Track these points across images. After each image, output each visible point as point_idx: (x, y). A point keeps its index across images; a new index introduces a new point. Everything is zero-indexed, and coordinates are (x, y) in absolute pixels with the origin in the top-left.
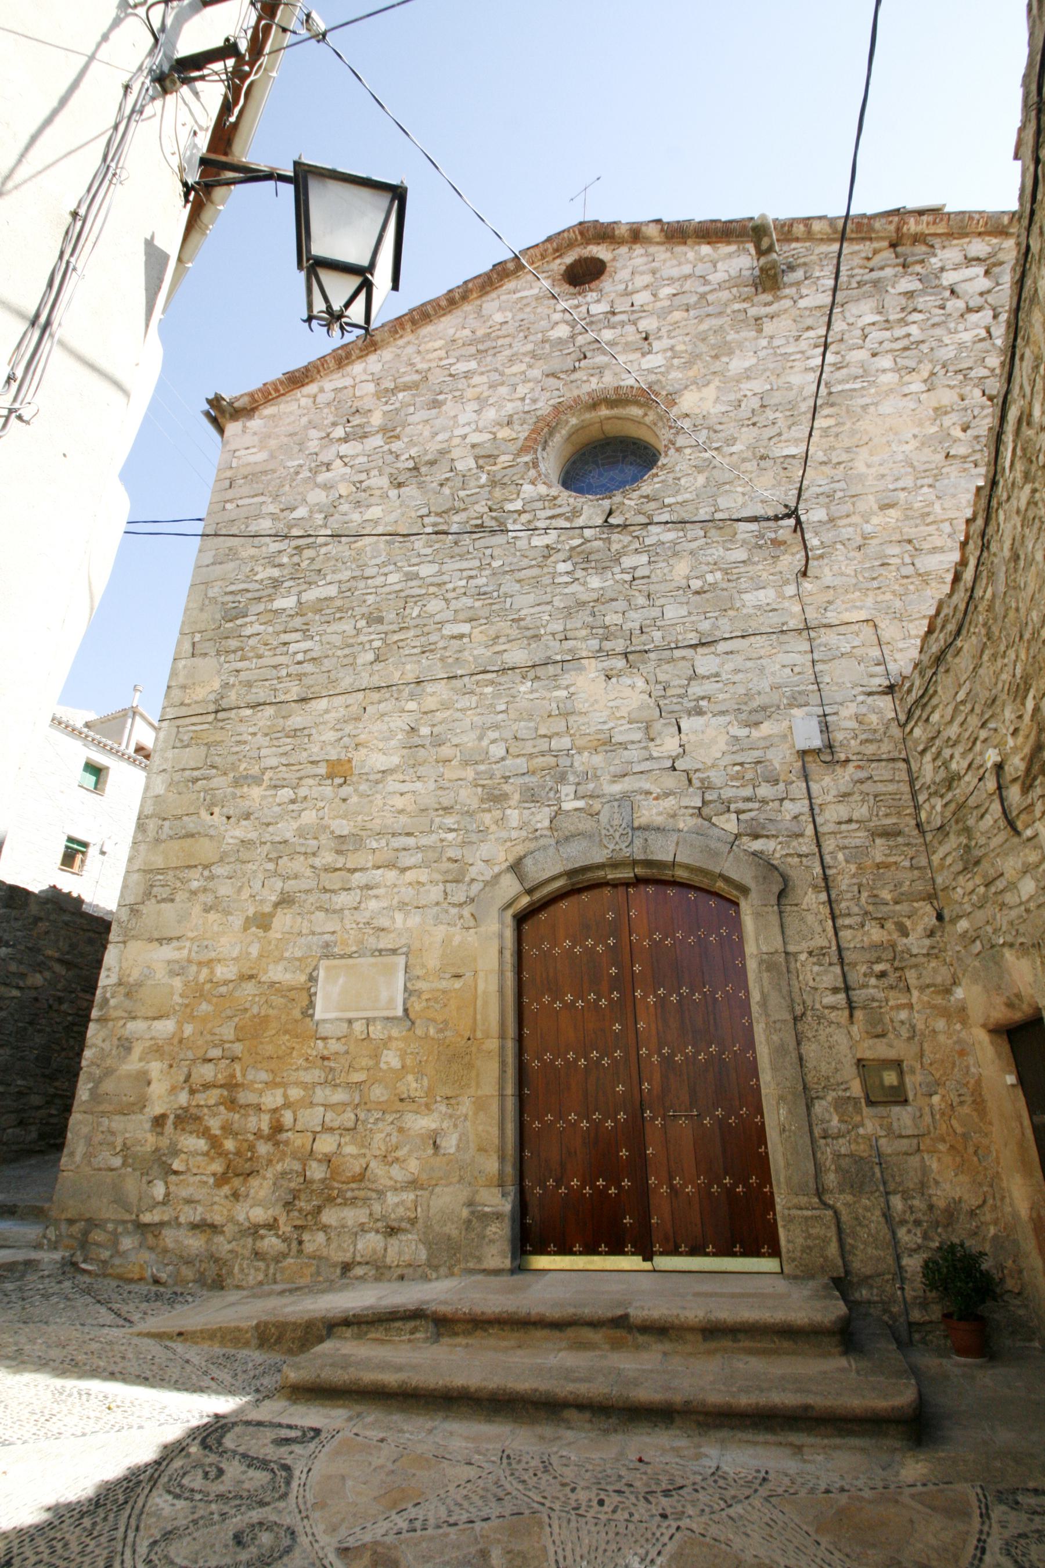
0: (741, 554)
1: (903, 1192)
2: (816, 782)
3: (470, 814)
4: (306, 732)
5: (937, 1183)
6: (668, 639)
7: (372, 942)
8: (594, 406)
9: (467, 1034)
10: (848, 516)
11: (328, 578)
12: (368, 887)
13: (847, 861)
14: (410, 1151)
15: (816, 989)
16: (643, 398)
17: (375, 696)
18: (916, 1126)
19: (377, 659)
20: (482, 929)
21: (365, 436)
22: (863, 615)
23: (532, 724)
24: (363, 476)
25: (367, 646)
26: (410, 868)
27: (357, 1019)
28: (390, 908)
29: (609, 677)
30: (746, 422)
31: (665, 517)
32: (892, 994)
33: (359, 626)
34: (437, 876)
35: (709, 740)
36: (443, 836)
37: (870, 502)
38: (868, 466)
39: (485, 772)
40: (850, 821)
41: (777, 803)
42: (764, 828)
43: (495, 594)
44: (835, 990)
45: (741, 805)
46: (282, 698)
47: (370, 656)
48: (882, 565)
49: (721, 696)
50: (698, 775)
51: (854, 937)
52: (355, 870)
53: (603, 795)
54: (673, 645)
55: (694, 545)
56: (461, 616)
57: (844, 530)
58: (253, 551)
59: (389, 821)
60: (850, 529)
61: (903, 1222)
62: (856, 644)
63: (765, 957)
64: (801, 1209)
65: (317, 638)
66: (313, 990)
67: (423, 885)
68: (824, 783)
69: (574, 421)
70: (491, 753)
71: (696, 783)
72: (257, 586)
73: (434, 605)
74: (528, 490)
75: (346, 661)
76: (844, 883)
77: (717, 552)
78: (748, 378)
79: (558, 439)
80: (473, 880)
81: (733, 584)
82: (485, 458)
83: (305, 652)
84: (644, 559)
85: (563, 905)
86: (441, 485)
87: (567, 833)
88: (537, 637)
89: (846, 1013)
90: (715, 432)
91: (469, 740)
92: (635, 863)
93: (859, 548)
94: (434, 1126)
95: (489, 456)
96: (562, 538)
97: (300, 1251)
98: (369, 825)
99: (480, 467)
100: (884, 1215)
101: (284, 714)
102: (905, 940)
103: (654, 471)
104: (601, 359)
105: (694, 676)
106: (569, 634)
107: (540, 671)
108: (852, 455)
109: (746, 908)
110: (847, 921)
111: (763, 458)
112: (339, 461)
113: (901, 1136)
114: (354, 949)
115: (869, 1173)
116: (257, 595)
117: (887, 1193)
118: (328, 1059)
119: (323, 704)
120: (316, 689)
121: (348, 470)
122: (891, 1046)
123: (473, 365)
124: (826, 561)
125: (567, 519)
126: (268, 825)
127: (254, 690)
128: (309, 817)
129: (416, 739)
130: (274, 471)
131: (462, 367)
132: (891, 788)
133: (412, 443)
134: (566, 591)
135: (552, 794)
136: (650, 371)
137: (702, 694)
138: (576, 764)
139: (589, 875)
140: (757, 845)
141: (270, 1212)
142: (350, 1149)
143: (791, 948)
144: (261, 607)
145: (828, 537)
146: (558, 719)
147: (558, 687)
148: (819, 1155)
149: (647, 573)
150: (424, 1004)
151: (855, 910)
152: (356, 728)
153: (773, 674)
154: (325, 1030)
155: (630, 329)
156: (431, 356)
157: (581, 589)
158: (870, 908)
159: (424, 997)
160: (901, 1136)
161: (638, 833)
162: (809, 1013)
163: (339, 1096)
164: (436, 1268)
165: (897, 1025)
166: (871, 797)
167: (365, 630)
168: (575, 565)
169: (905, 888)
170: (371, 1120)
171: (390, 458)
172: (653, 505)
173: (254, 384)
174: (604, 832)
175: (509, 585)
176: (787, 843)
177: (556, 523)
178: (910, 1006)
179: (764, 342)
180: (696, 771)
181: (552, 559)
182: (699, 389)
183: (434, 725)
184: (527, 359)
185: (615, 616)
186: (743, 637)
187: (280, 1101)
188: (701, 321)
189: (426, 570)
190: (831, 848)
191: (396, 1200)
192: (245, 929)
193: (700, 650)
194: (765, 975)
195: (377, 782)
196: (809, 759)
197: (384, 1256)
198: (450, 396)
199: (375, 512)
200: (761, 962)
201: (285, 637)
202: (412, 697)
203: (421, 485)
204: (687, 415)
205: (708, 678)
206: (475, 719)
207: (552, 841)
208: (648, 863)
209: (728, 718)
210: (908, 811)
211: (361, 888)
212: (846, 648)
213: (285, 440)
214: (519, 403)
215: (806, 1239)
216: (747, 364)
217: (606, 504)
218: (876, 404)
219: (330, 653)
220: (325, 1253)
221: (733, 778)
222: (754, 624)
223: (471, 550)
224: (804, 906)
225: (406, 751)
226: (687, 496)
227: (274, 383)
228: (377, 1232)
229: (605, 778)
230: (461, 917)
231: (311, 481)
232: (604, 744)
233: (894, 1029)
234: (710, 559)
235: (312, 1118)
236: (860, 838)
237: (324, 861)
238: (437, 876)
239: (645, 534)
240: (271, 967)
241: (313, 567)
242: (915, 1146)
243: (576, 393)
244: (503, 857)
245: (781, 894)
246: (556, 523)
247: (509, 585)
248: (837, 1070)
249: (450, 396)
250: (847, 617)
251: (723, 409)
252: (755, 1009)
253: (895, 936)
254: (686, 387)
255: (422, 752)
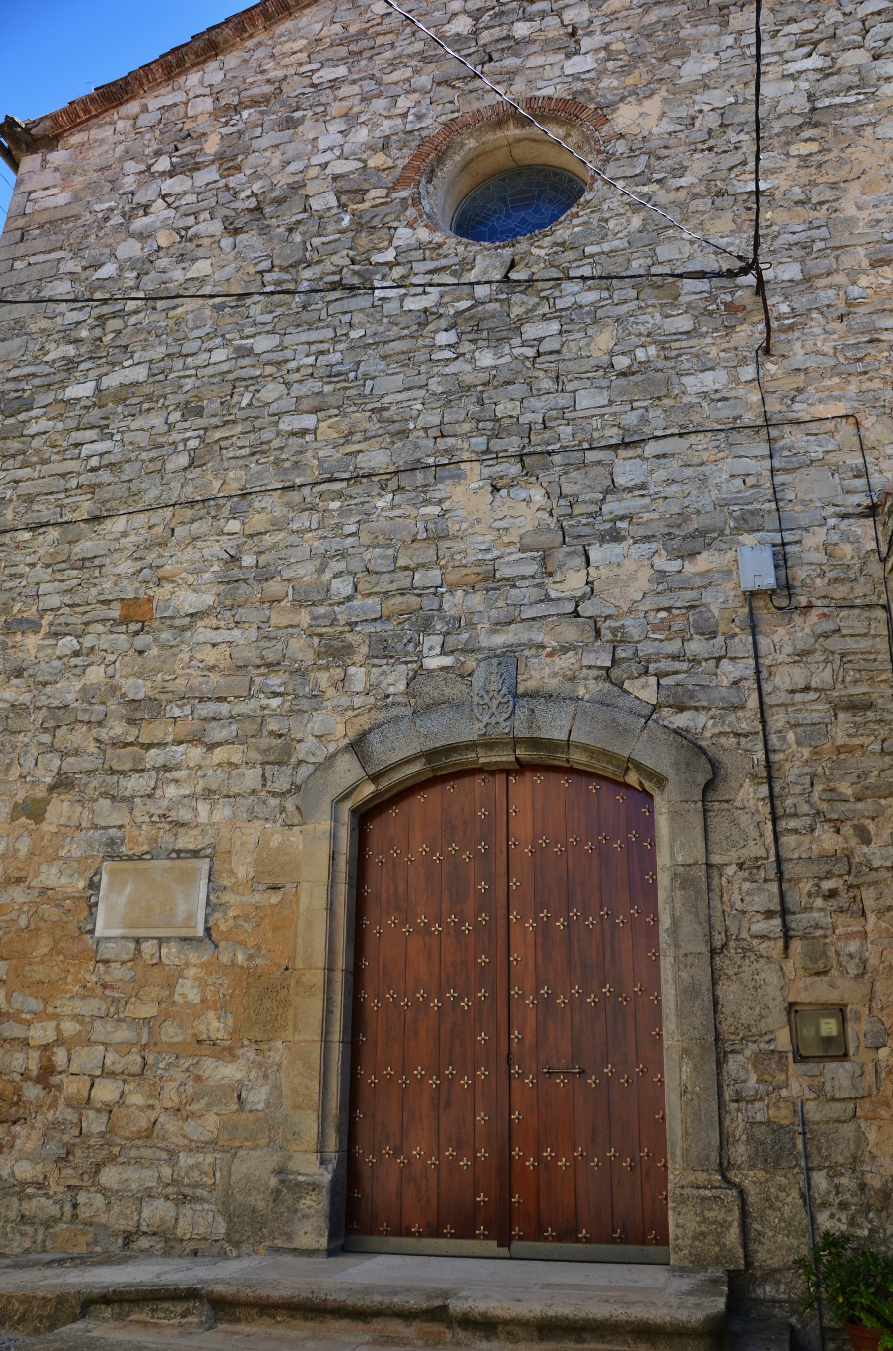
0: (684, 323)
1: (830, 1168)
2: (767, 635)
3: (301, 673)
4: (97, 562)
5: (873, 1157)
6: (580, 436)
7: (167, 840)
8: (499, 123)
9: (284, 963)
10: (828, 275)
11: (136, 356)
12: (166, 768)
13: (799, 743)
14: (209, 1106)
15: (744, 913)
16: (567, 111)
17: (189, 513)
18: (854, 1087)
19: (192, 465)
20: (309, 827)
21: (197, 167)
22: (841, 408)
23: (391, 552)
24: (191, 220)
25: (181, 447)
26: (220, 744)
27: (147, 939)
28: (193, 796)
29: (495, 489)
30: (700, 146)
31: (587, 271)
32: (842, 919)
33: (171, 419)
34: (254, 756)
35: (626, 573)
36: (265, 701)
37: (860, 256)
38: (859, 208)
39: (324, 616)
40: (807, 689)
41: (712, 663)
42: (691, 697)
43: (352, 375)
44: (769, 914)
45: (665, 665)
46: (70, 517)
47: (183, 460)
48: (870, 341)
49: (646, 516)
50: (608, 623)
51: (800, 845)
52: (150, 746)
53: (480, 649)
54: (586, 445)
55: (623, 309)
56: (305, 405)
57: (822, 294)
58: (44, 324)
59: (196, 682)
60: (831, 292)
61: (824, 1205)
62: (830, 447)
63: (681, 870)
64: (698, 1187)
65: (117, 437)
66: (93, 900)
67: (236, 766)
68: (776, 637)
69: (471, 143)
70: (333, 591)
71: (606, 634)
72: (47, 369)
73: (271, 391)
74: (404, 236)
75: (152, 467)
76: (792, 773)
77: (653, 319)
78: (706, 87)
79: (449, 167)
80: (300, 762)
81: (672, 363)
82: (349, 191)
83: (101, 455)
84: (554, 327)
85: (421, 798)
86: (290, 230)
87: (428, 700)
88: (404, 433)
89: (780, 943)
90: (659, 158)
91: (305, 572)
92: (516, 742)
93: (841, 318)
94: (239, 1075)
95: (355, 191)
96: (446, 299)
97: (75, 1216)
98: (170, 686)
99: (342, 206)
100: (802, 1196)
101: (70, 538)
102: (865, 849)
103: (574, 210)
104: (511, 62)
105: (612, 489)
106: (447, 429)
107: (406, 480)
108: (838, 193)
109: (661, 803)
110: (792, 824)
111: (720, 194)
112: (160, 201)
113: (834, 1100)
114: (146, 848)
115: (792, 1146)
116: (46, 381)
117: (809, 1170)
118: (112, 987)
119: (119, 524)
120: (114, 504)
121: (171, 213)
122: (833, 986)
123: (341, 71)
124: (797, 334)
125: (454, 274)
126: (45, 684)
127: (35, 507)
128: (96, 674)
129: (236, 571)
130: (77, 217)
131: (329, 74)
132: (864, 644)
133: (256, 175)
134: (447, 370)
135: (410, 648)
136: (575, 77)
137: (621, 512)
138: (446, 607)
139: (456, 758)
140: (681, 720)
141: (39, 1168)
142: (136, 1099)
143: (716, 859)
144: (50, 397)
145: (801, 302)
146: (424, 544)
147: (427, 502)
148: (727, 1123)
149: (557, 347)
150: (231, 923)
151: (804, 808)
152: (160, 556)
153: (718, 486)
154: (108, 950)
155: (553, 21)
156: (287, 61)
157: (468, 367)
158: (824, 806)
159: (231, 913)
160: (834, 1100)
161: (523, 702)
162: (732, 944)
163: (123, 1034)
164: (237, 1245)
165: (844, 959)
166: (837, 657)
167: (178, 426)
168: (460, 336)
169: (872, 779)
170: (162, 1065)
171: (225, 197)
172: (570, 255)
173: (57, 103)
174: (476, 699)
175: (371, 363)
176: (722, 717)
177: (436, 279)
178: (864, 935)
179: (729, 40)
180: (607, 617)
181: (431, 327)
182: (639, 102)
183: (261, 553)
184: (414, 63)
185: (510, 405)
186: (681, 435)
187: (51, 1036)
188: (647, 12)
189: (263, 344)
190: (780, 725)
191: (191, 1162)
192: (13, 819)
193: (622, 453)
194: (678, 893)
195: (183, 629)
196: (759, 603)
197: (175, 1227)
198: (309, 113)
199: (202, 268)
200: (675, 876)
201: (77, 436)
202: (234, 514)
203: (264, 231)
204: (622, 136)
205: (630, 490)
206: (316, 544)
207: (408, 711)
208: (535, 743)
209: (654, 546)
210: (884, 677)
211: (157, 770)
212: (816, 452)
213: (95, 176)
214: (399, 121)
215: (699, 1223)
216: (705, 69)
217: (508, 252)
218: (875, 124)
219: (133, 456)
220: (103, 1219)
221: (656, 629)
222: (696, 418)
223: (324, 315)
224: (738, 804)
225: (222, 587)
226: (616, 244)
227: (83, 101)
228: (167, 1198)
229: (483, 627)
230: (283, 810)
231: (125, 229)
232: (486, 579)
233: (840, 964)
234: (642, 329)
235: (87, 1059)
236: (818, 711)
237: (111, 734)
238: (254, 756)
239: (557, 293)
240: (43, 868)
241: (119, 342)
242: (850, 1112)
243: (476, 105)
244: (341, 731)
245: (709, 787)
246: (436, 279)
247: (371, 363)
248: (761, 1016)
249: (309, 113)
250: (821, 410)
251: (671, 128)
252: (664, 937)
253: (854, 842)
254: (622, 99)
255: (243, 588)
